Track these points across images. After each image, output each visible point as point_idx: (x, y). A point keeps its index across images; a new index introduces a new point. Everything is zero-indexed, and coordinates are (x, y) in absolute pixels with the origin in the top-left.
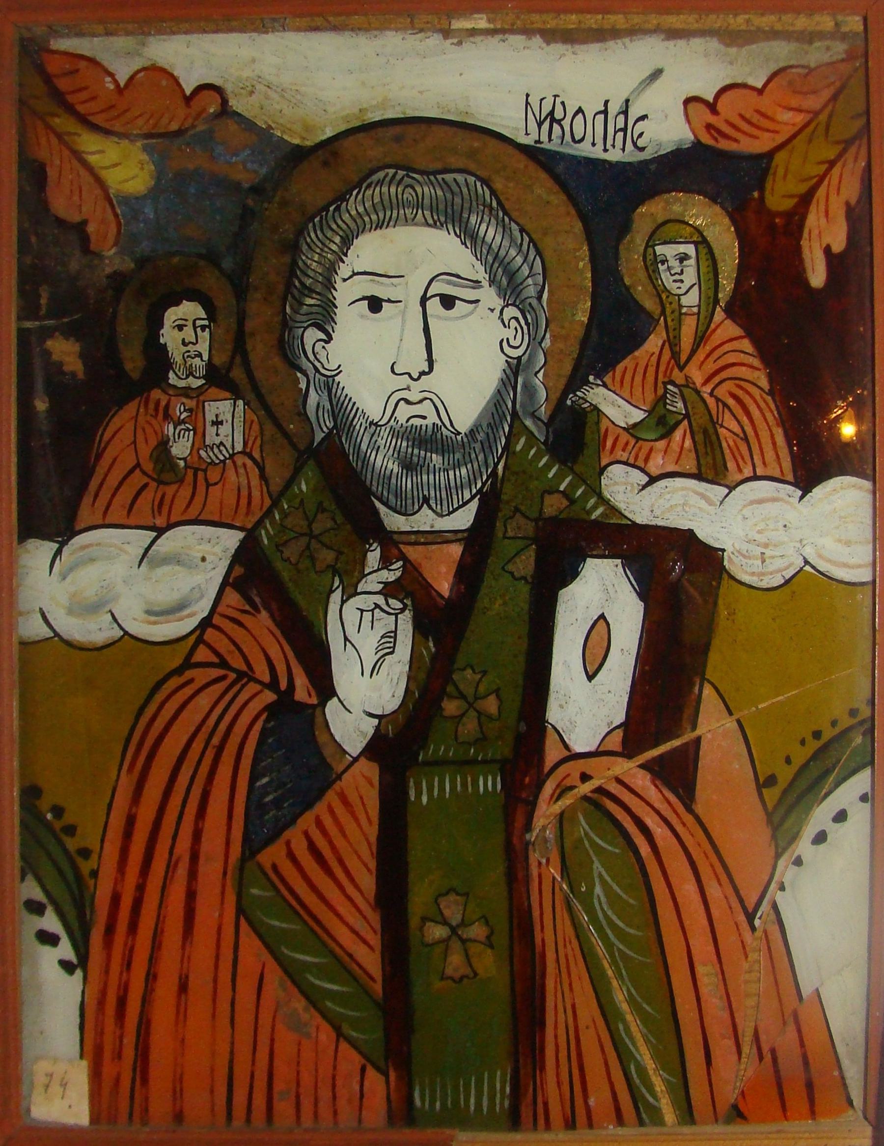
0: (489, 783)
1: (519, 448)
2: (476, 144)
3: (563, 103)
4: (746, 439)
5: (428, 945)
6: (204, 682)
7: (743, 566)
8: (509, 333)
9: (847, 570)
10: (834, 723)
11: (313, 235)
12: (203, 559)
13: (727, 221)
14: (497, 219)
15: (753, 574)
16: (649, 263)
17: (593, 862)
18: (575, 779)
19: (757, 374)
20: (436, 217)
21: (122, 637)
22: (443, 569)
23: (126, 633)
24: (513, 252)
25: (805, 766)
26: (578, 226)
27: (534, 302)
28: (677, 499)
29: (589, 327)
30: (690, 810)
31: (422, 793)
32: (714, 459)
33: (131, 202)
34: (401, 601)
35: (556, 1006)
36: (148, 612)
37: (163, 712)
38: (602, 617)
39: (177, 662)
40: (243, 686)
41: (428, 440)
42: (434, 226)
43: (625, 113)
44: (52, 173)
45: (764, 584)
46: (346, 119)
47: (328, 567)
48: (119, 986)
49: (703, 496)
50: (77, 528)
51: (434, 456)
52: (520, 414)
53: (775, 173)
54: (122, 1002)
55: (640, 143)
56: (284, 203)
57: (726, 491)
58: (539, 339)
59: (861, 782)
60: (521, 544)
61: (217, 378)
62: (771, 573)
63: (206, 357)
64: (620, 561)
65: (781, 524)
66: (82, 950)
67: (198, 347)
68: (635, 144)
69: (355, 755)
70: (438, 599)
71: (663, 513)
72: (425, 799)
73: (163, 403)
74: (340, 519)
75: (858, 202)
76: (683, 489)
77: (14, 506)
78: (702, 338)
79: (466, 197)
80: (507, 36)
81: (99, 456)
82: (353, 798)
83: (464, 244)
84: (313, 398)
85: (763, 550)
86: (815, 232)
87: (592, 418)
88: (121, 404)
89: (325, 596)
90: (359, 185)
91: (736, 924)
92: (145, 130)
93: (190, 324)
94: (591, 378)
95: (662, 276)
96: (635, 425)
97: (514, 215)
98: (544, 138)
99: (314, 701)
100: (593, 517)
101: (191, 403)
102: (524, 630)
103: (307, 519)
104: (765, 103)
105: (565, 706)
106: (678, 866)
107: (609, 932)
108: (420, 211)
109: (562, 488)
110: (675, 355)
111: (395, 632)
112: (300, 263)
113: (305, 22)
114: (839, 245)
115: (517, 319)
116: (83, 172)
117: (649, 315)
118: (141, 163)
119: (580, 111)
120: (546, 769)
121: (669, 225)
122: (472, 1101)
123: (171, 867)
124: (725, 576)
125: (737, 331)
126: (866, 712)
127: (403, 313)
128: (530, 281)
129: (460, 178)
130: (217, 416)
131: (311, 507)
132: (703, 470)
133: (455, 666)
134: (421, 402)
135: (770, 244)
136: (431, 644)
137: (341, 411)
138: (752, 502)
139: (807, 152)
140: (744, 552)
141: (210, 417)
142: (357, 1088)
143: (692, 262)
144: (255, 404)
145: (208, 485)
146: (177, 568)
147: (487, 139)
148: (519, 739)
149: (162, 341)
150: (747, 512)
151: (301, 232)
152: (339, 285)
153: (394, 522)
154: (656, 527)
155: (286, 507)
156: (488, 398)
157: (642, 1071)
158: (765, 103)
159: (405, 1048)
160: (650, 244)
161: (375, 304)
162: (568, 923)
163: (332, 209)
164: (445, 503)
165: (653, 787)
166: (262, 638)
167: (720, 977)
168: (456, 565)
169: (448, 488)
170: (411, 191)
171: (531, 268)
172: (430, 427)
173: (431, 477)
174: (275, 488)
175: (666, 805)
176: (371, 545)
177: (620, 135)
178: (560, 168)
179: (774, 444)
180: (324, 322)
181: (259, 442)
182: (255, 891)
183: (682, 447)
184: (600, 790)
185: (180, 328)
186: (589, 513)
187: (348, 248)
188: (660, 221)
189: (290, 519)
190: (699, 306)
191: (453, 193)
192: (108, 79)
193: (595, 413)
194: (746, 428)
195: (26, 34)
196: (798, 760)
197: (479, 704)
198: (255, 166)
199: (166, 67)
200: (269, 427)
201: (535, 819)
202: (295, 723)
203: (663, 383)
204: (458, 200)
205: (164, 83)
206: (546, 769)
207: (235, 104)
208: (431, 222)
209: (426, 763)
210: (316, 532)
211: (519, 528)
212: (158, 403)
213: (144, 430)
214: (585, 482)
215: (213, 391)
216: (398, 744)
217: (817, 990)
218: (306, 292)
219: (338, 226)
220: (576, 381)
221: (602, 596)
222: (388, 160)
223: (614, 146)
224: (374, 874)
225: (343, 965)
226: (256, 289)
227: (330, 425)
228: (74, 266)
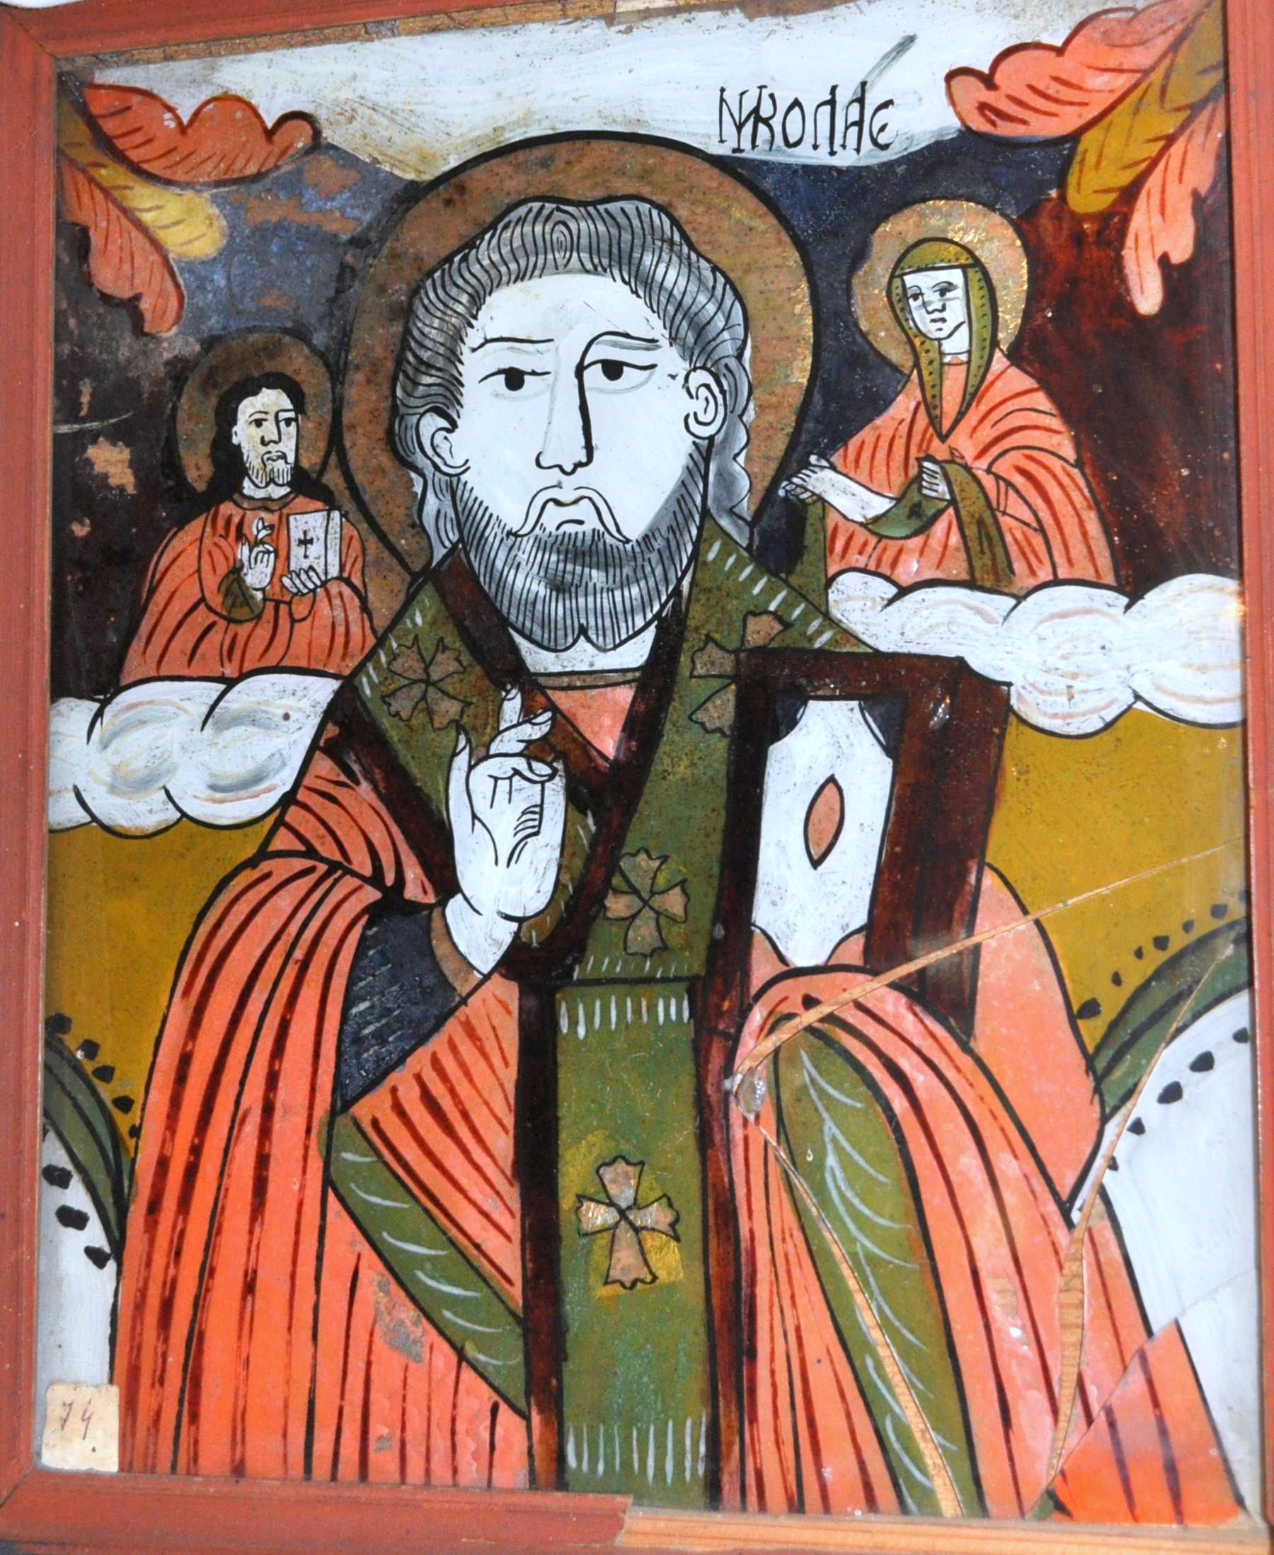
0: (672, 1009)
1: (711, 556)
2: (651, 161)
3: (772, 96)
4: (1042, 530)
5: (586, 1234)
6: (285, 876)
7: (1037, 702)
8: (698, 406)
9: (1202, 706)
10: (1187, 927)
11: (432, 295)
12: (286, 717)
13: (1010, 232)
14: (680, 257)
15: (1055, 716)
16: (895, 298)
17: (823, 1120)
18: (795, 1004)
19: (1056, 439)
20: (596, 261)
21: (179, 820)
22: (607, 721)
23: (184, 814)
24: (702, 299)
25: (1144, 988)
26: (794, 257)
27: (733, 363)
28: (940, 615)
29: (809, 392)
30: (967, 1049)
31: (579, 1022)
32: (994, 559)
33: (199, 270)
34: (550, 765)
35: (772, 1328)
36: (213, 788)
37: (230, 917)
38: (832, 780)
39: (250, 850)
40: (336, 881)
41: (586, 551)
42: (595, 271)
43: (861, 100)
44: (96, 240)
45: (1073, 730)
46: (476, 141)
47: (451, 721)
48: (165, 1283)
49: (978, 611)
50: (124, 682)
51: (594, 572)
52: (713, 511)
53: (1082, 161)
54: (167, 1306)
55: (882, 139)
56: (395, 256)
57: (1013, 602)
58: (739, 410)
59: (1234, 1013)
60: (716, 684)
61: (306, 484)
62: (1083, 714)
63: (291, 458)
64: (855, 704)
65: (1096, 646)
66: (117, 1234)
67: (281, 447)
68: (874, 141)
69: (486, 971)
70: (600, 761)
71: (919, 636)
72: (581, 1031)
73: (236, 520)
74: (466, 658)
75: (1213, 187)
76: (948, 602)
77: (47, 655)
78: (973, 396)
79: (638, 230)
80: (694, 14)
81: (152, 591)
82: (483, 1031)
83: (635, 292)
84: (432, 504)
85: (1070, 682)
86: (1144, 238)
87: (815, 511)
88: (182, 523)
89: (446, 760)
90: (493, 226)
91: (1043, 1217)
92: (214, 176)
93: (271, 417)
94: (813, 459)
95: (916, 315)
96: (877, 519)
97: (703, 248)
98: (746, 144)
99: (431, 899)
100: (817, 645)
101: (271, 518)
102: (721, 800)
103: (423, 660)
104: (1065, 67)
105: (779, 903)
106: (951, 1131)
107: (848, 1220)
108: (575, 254)
109: (772, 607)
110: (934, 421)
111: (541, 806)
112: (416, 333)
113: (418, 23)
114: (1181, 249)
115: (707, 387)
116: (134, 233)
117: (895, 369)
118: (209, 218)
119: (797, 103)
120: (754, 990)
121: (926, 245)
122: (651, 1462)
123: (237, 1122)
124: (1013, 719)
125: (1029, 383)
126: (1237, 909)
127: (552, 389)
128: (726, 335)
129: (629, 206)
130: (305, 533)
131: (428, 646)
132: (978, 575)
133: (625, 850)
134: (576, 502)
135: (1075, 264)
136: (590, 821)
137: (469, 521)
138: (1052, 617)
139: (1131, 128)
140: (1041, 686)
141: (296, 534)
142: (486, 1436)
143: (959, 293)
144: (355, 515)
145: (293, 621)
146: (252, 729)
147: (665, 152)
148: (714, 947)
149: (235, 441)
150: (1044, 630)
151: (415, 292)
152: (466, 356)
153: (538, 660)
154: (909, 656)
155: (395, 645)
156: (668, 492)
157: (903, 1431)
158: (1065, 67)
159: (554, 1382)
160: (897, 272)
161: (514, 379)
162: (787, 1206)
163: (457, 259)
164: (609, 633)
165: (910, 1017)
166: (363, 818)
167: (1021, 1295)
168: (623, 717)
169: (614, 614)
170: (562, 228)
171: (728, 319)
172: (589, 534)
173: (591, 599)
174: (381, 622)
175: (930, 1041)
176: (508, 692)
177: (854, 131)
178: (768, 183)
179: (1085, 534)
180: (447, 404)
181: (359, 565)
182: (348, 1156)
183: (946, 547)
184: (831, 1018)
185: (259, 423)
186: (811, 639)
187: (479, 309)
188: (911, 241)
189: (400, 661)
190: (969, 352)
191: (619, 227)
192: (168, 115)
193: (819, 505)
194: (1041, 514)
195: (67, 67)
196: (1133, 981)
197: (657, 902)
198: (357, 212)
199: (240, 94)
200: (373, 543)
201: (738, 1061)
202: (404, 926)
203: (918, 459)
204: (626, 236)
205: (239, 115)
206: (754, 990)
207: (329, 135)
208: (589, 266)
209: (583, 983)
210: (435, 676)
211: (713, 664)
212: (229, 521)
213: (210, 554)
214: (805, 598)
215: (301, 501)
216: (545, 959)
217: (1177, 1323)
218: (423, 369)
219: (465, 281)
220: (793, 461)
221: (832, 752)
222: (531, 191)
223: (844, 146)
224: (512, 1132)
225: (466, 1259)
226: (357, 368)
227: (454, 537)
228: (124, 353)
